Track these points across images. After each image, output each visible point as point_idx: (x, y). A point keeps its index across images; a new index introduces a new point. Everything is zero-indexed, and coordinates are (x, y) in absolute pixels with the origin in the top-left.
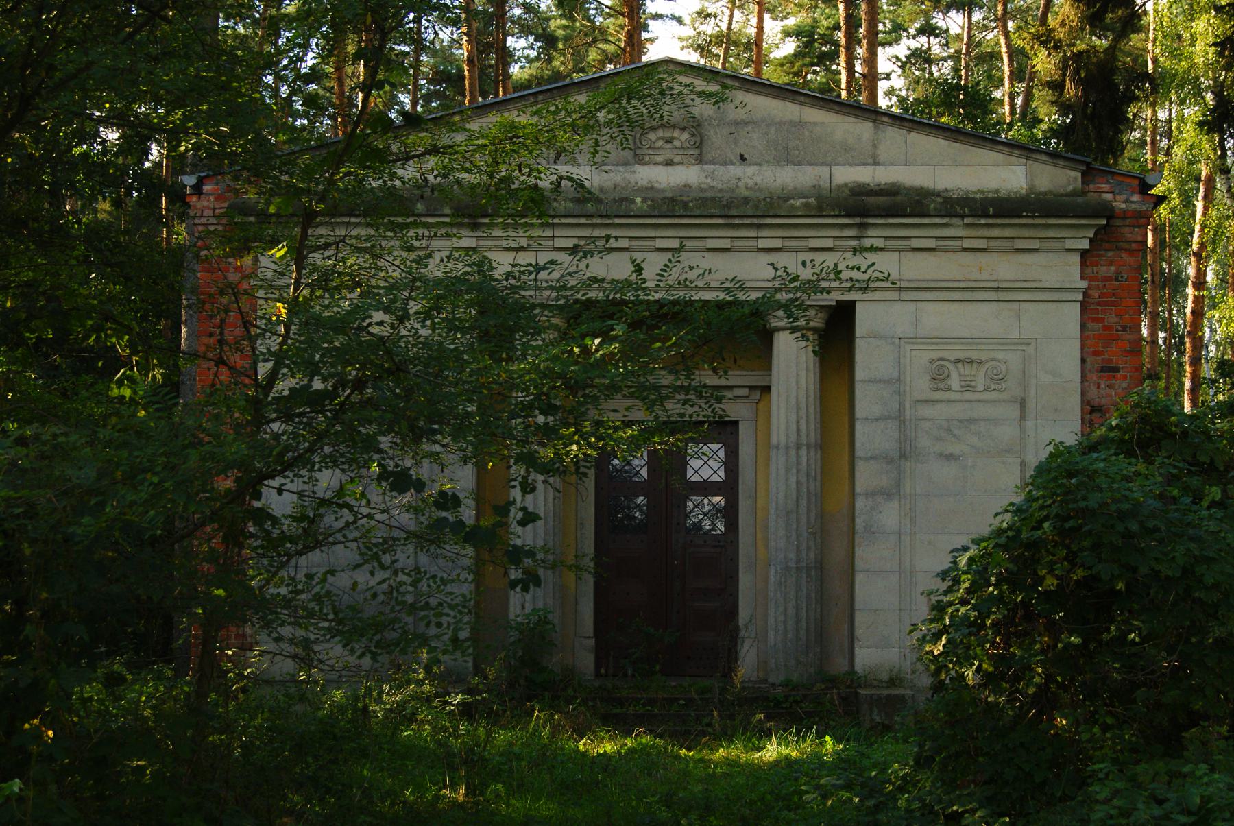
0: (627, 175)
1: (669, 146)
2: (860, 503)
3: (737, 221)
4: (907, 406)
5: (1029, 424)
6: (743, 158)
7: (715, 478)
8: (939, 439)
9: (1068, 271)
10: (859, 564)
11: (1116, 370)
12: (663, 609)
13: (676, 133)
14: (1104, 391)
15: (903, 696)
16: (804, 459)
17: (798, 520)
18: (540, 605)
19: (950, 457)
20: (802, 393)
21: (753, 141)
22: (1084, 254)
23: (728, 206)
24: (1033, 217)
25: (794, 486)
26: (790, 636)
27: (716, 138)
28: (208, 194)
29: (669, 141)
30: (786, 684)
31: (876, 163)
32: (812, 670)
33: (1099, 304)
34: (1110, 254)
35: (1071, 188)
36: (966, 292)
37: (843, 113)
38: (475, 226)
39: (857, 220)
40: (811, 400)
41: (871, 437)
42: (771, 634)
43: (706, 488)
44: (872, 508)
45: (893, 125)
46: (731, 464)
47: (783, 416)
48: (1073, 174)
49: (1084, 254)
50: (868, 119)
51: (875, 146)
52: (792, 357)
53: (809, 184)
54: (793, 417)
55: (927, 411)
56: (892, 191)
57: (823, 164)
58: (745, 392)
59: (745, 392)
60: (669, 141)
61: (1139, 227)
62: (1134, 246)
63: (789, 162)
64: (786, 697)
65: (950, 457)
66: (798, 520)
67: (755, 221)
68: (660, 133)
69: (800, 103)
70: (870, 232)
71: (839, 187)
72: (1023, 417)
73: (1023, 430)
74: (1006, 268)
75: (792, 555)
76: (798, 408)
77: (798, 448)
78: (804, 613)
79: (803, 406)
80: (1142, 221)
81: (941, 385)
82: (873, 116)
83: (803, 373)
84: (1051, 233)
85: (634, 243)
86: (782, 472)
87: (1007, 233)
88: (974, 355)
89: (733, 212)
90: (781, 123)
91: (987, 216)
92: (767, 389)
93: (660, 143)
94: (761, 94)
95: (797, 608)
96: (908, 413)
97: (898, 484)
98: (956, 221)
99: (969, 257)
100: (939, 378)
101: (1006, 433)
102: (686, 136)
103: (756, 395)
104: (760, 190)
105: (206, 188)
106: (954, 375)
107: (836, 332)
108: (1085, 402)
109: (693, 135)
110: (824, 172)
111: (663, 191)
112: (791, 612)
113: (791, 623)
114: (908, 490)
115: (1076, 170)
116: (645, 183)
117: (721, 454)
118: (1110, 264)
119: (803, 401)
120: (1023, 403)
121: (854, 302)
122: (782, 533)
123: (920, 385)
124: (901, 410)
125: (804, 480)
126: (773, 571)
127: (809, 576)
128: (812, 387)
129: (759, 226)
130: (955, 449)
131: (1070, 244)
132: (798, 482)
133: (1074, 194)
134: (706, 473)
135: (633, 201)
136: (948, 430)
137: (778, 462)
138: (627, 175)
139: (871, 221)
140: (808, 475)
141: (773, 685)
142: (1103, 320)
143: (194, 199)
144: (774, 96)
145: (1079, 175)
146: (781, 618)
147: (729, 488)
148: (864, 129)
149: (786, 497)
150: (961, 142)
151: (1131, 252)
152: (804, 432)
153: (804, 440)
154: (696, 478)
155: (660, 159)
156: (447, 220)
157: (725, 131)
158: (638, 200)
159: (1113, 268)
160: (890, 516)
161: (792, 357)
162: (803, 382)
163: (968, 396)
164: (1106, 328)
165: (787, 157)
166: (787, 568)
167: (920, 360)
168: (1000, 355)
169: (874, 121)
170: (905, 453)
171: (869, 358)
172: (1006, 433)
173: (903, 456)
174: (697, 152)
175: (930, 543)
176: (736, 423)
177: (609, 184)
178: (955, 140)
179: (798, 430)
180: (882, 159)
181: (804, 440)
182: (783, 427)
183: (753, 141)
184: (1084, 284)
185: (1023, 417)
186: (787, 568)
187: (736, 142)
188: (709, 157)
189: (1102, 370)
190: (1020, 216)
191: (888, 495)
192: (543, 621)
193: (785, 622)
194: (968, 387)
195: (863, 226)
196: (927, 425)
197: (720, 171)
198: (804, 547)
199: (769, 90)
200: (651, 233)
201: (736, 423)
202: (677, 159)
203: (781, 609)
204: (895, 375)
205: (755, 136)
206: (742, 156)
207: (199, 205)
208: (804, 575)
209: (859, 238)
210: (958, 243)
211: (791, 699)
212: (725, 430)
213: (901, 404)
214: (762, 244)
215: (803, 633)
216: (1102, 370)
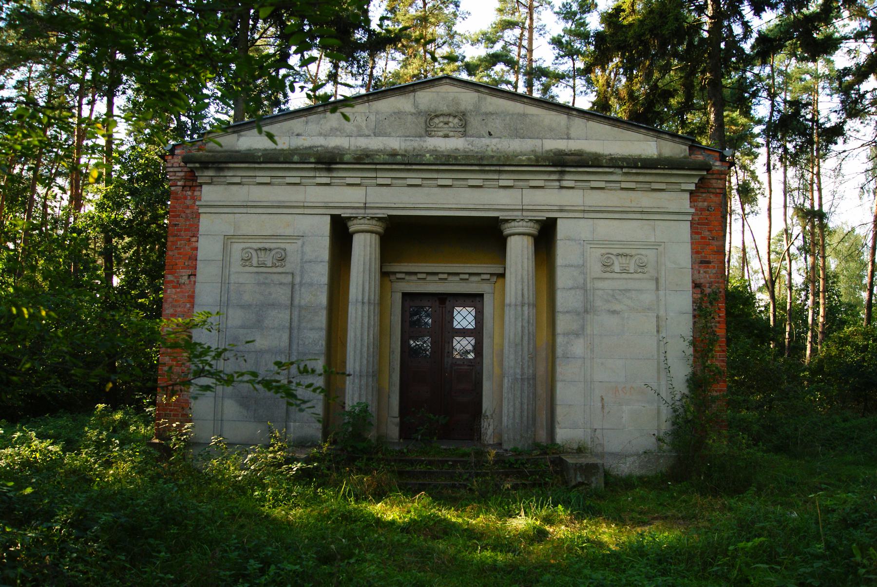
0: (422, 143)
1: (446, 126)
2: (560, 340)
3: (487, 168)
4: (588, 281)
5: (661, 293)
6: (490, 134)
7: (470, 327)
8: (608, 301)
9: (683, 202)
10: (559, 376)
11: (709, 262)
12: (436, 417)
13: (451, 119)
14: (702, 275)
15: (597, 464)
16: (526, 313)
17: (522, 350)
18: (364, 400)
19: (614, 312)
20: (525, 273)
21: (496, 125)
22: (691, 192)
23: (482, 158)
24: (664, 169)
25: (520, 329)
26: (517, 421)
27: (474, 122)
28: (177, 155)
29: (446, 123)
30: (515, 450)
31: (569, 138)
32: (530, 442)
33: (698, 224)
34: (704, 195)
35: (682, 155)
36: (622, 214)
37: (549, 109)
38: (329, 170)
39: (559, 169)
40: (530, 278)
41: (565, 299)
42: (505, 419)
43: (464, 333)
44: (568, 343)
45: (579, 117)
46: (479, 318)
47: (513, 285)
48: (684, 147)
49: (691, 192)
50: (564, 113)
51: (568, 128)
52: (519, 250)
53: (529, 149)
54: (520, 287)
55: (600, 284)
56: (580, 153)
57: (537, 138)
58: (488, 277)
59: (488, 277)
60: (446, 123)
61: (721, 179)
62: (718, 191)
63: (517, 136)
64: (516, 460)
65: (614, 312)
66: (522, 350)
67: (498, 168)
68: (441, 119)
69: (524, 103)
70: (567, 177)
71: (547, 152)
72: (657, 289)
73: (658, 297)
74: (646, 200)
75: (518, 371)
76: (523, 282)
77: (523, 305)
78: (525, 407)
79: (526, 280)
80: (723, 176)
81: (609, 269)
82: (567, 111)
83: (526, 261)
84: (673, 180)
85: (425, 182)
86: (513, 320)
87: (648, 179)
88: (627, 251)
89: (485, 162)
90: (512, 114)
91: (636, 167)
92: (503, 275)
93: (441, 124)
94: (501, 97)
95: (522, 404)
96: (589, 285)
97: (583, 328)
98: (618, 171)
99: (624, 193)
100: (607, 266)
101: (648, 298)
102: (456, 120)
103: (494, 279)
104: (501, 152)
105: (177, 152)
106: (616, 263)
107: (545, 235)
108: (693, 282)
109: (461, 120)
110: (538, 142)
111: (442, 152)
112: (518, 405)
113: (518, 413)
114: (589, 332)
115: (686, 145)
116: (432, 147)
117: (473, 313)
118: (704, 201)
119: (526, 277)
120: (657, 280)
121: (555, 219)
122: (512, 357)
123: (596, 269)
124: (585, 284)
125: (526, 325)
126: (506, 380)
127: (529, 383)
128: (530, 269)
129: (500, 172)
130: (617, 307)
131: (684, 187)
132: (522, 326)
133: (685, 157)
134: (464, 324)
135: (425, 156)
136: (613, 296)
137: (510, 314)
138: (422, 143)
139: (568, 169)
140: (528, 322)
141: (506, 450)
142: (701, 233)
143: (170, 157)
144: (509, 99)
145: (687, 148)
146: (511, 409)
147: (477, 333)
148: (561, 119)
149: (515, 334)
150: (619, 127)
151: (716, 194)
152: (526, 296)
153: (526, 301)
154: (459, 327)
155: (441, 134)
156: (312, 166)
157: (480, 118)
158: (428, 155)
159: (706, 204)
160: (578, 347)
161: (519, 250)
162: (526, 265)
163: (624, 276)
164: (702, 238)
165: (517, 134)
166: (516, 379)
167: (595, 255)
168: (643, 252)
169: (568, 114)
170: (587, 310)
171: (565, 252)
172: (648, 298)
173: (586, 311)
174: (463, 130)
175: (602, 364)
176: (482, 295)
177: (410, 148)
178: (615, 126)
179: (523, 295)
180: (572, 135)
181: (526, 301)
182: (513, 293)
183: (496, 125)
184: (693, 210)
185: (657, 289)
186: (516, 379)
187: (486, 125)
188: (470, 133)
189: (701, 262)
190: (656, 168)
191: (577, 335)
192: (365, 410)
193: (514, 413)
194: (624, 271)
195: (562, 173)
196: (599, 293)
197: (476, 141)
198: (526, 365)
199: (505, 95)
200: (435, 176)
201: (482, 295)
202: (451, 134)
203: (512, 404)
204: (581, 262)
205: (497, 121)
206: (490, 133)
207: (172, 161)
208: (526, 383)
209: (559, 180)
210: (618, 185)
211: (519, 462)
212: (474, 299)
213: (585, 280)
214: (502, 183)
215: (525, 418)
216: (701, 262)
